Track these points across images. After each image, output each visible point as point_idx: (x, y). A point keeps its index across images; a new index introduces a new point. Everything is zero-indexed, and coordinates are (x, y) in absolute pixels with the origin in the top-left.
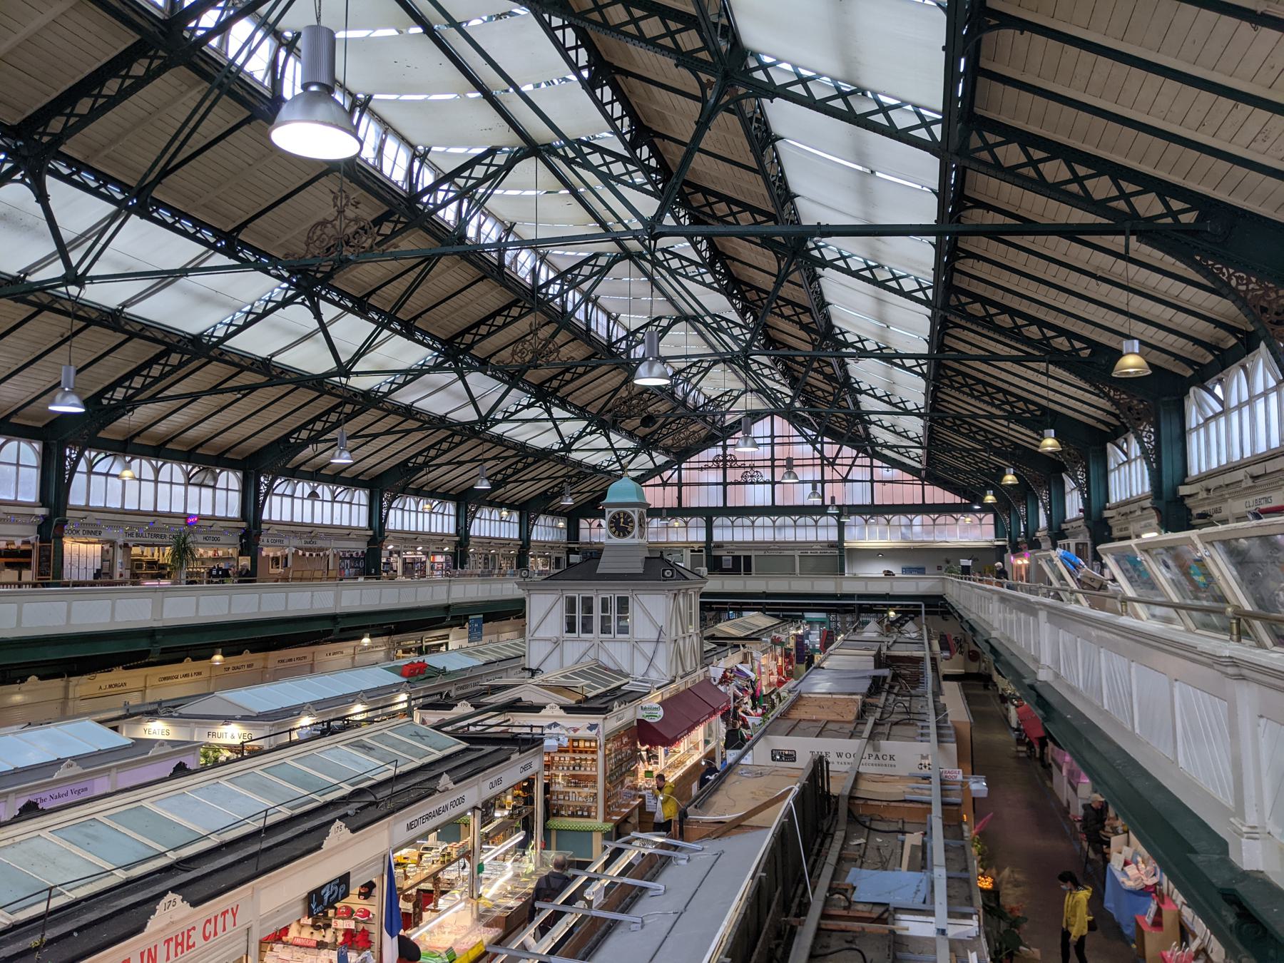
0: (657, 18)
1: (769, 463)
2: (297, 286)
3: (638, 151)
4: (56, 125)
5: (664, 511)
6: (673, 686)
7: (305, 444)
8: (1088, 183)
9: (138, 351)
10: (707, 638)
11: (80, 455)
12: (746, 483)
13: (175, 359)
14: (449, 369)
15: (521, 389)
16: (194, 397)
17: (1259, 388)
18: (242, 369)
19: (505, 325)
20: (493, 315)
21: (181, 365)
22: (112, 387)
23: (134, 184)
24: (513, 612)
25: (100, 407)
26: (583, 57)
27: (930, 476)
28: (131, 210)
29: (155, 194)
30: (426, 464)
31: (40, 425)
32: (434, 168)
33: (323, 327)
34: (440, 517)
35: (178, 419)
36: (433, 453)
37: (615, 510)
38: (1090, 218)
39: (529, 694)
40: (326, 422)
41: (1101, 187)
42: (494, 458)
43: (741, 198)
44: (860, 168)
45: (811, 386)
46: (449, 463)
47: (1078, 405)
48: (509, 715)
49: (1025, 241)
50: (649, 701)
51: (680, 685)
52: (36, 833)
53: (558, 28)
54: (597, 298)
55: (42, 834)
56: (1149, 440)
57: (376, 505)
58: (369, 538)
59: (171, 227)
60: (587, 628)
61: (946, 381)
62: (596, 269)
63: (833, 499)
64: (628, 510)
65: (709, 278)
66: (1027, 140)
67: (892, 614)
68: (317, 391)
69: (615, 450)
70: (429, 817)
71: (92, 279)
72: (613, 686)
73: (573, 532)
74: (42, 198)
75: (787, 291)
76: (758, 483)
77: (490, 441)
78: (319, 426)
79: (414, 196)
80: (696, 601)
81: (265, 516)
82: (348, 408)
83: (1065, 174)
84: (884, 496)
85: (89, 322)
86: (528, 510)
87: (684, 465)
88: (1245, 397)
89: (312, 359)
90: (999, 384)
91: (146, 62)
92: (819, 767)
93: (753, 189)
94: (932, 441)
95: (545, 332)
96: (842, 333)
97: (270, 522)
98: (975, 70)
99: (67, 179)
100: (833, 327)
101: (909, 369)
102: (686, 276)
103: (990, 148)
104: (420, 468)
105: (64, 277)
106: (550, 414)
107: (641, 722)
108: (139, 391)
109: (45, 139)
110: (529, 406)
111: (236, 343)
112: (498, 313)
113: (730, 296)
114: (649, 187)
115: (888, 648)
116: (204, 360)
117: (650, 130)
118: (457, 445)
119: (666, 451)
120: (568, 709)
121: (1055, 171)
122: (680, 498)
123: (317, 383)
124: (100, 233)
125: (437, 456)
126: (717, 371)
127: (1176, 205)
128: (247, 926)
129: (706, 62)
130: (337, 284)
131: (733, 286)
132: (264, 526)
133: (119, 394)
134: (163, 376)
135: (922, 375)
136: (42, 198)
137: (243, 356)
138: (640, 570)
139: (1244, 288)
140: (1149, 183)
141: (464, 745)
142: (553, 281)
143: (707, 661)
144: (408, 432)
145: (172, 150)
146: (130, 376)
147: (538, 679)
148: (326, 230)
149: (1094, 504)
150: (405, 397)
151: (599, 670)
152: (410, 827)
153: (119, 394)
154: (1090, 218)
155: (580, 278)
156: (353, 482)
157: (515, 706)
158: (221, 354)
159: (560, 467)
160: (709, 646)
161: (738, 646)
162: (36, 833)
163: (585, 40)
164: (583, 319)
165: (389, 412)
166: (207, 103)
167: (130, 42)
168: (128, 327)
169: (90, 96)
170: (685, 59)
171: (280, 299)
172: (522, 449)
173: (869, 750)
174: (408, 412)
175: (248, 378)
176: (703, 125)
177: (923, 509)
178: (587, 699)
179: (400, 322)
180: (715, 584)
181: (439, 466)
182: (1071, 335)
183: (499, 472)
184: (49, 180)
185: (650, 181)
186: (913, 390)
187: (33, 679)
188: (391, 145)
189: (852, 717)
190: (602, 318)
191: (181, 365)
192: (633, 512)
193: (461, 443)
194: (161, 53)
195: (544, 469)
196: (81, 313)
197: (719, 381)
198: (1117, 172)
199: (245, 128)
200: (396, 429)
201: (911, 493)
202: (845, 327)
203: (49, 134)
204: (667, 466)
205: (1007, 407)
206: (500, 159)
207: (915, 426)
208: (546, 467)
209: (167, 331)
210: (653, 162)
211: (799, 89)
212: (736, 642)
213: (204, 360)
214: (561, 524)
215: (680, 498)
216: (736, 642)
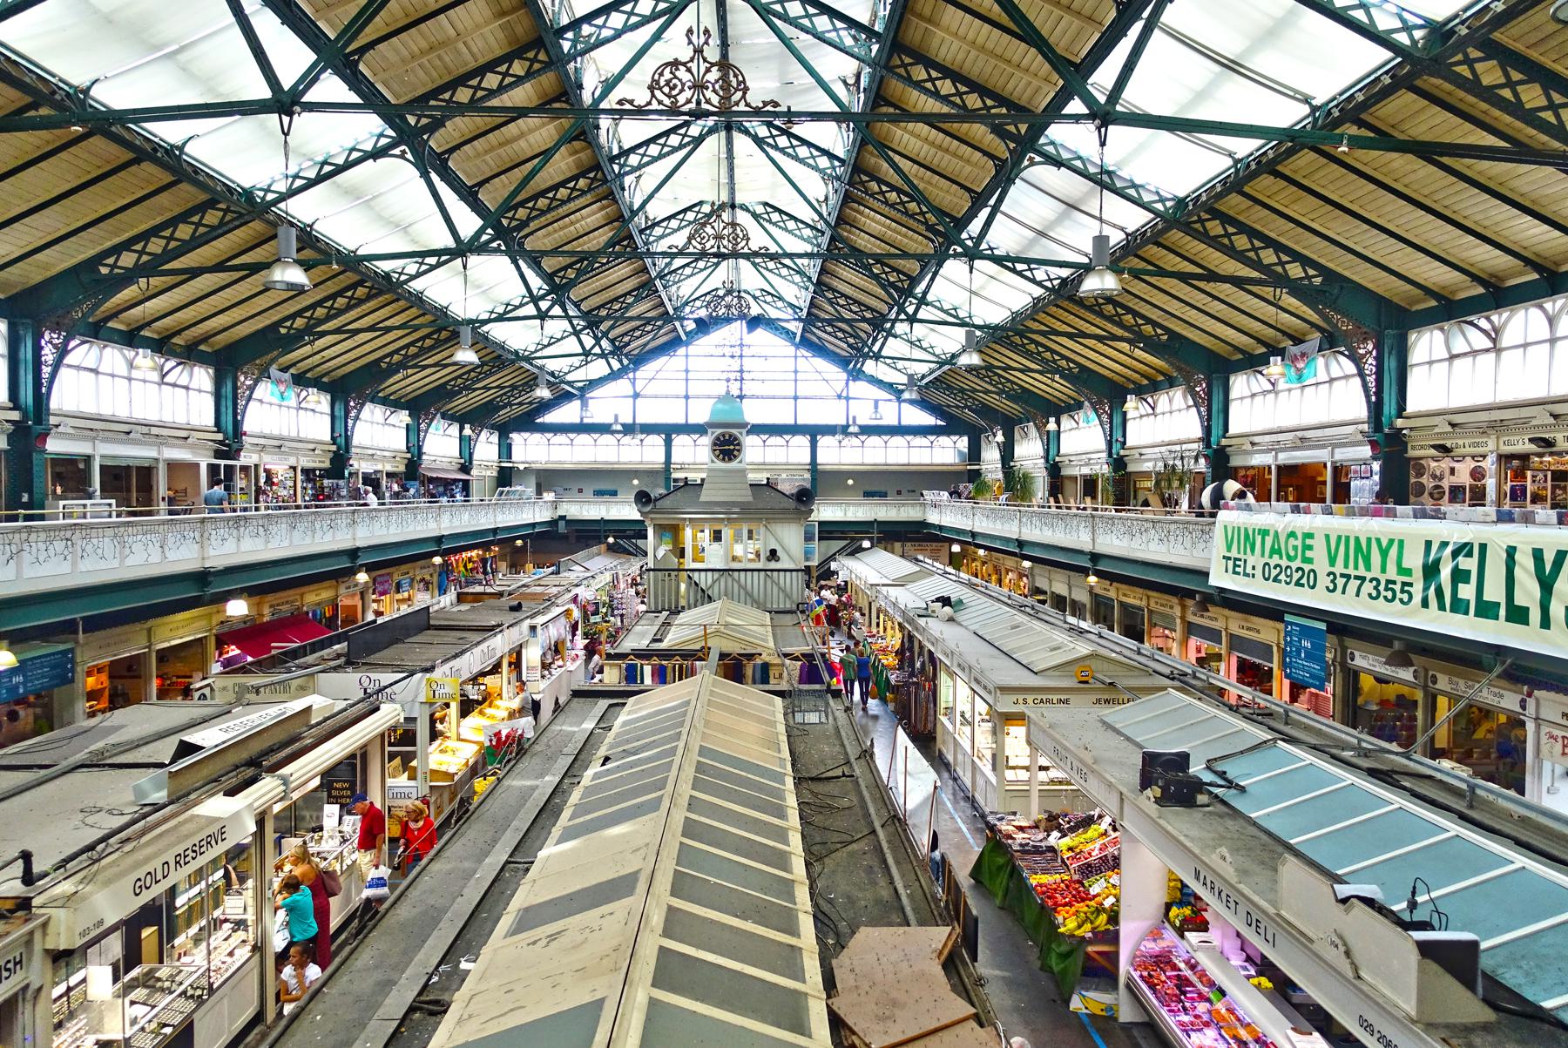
7: (129, 277)
13: (212, 217)
14: (497, 250)
16: (194, 273)
37: (719, 431)
38: (1255, 274)
40: (170, 238)
41: (1268, 256)
49: (1209, 287)
58: (331, 455)
62: (687, 140)
63: (854, 418)
78: (156, 246)
101: (1020, 274)
102: (776, 147)
121: (1242, 242)
125: (328, 318)
127: (1311, 272)
140: (1297, 257)
148: (677, 73)
154: (1255, 274)
182: (1068, 359)
198: (1279, 247)
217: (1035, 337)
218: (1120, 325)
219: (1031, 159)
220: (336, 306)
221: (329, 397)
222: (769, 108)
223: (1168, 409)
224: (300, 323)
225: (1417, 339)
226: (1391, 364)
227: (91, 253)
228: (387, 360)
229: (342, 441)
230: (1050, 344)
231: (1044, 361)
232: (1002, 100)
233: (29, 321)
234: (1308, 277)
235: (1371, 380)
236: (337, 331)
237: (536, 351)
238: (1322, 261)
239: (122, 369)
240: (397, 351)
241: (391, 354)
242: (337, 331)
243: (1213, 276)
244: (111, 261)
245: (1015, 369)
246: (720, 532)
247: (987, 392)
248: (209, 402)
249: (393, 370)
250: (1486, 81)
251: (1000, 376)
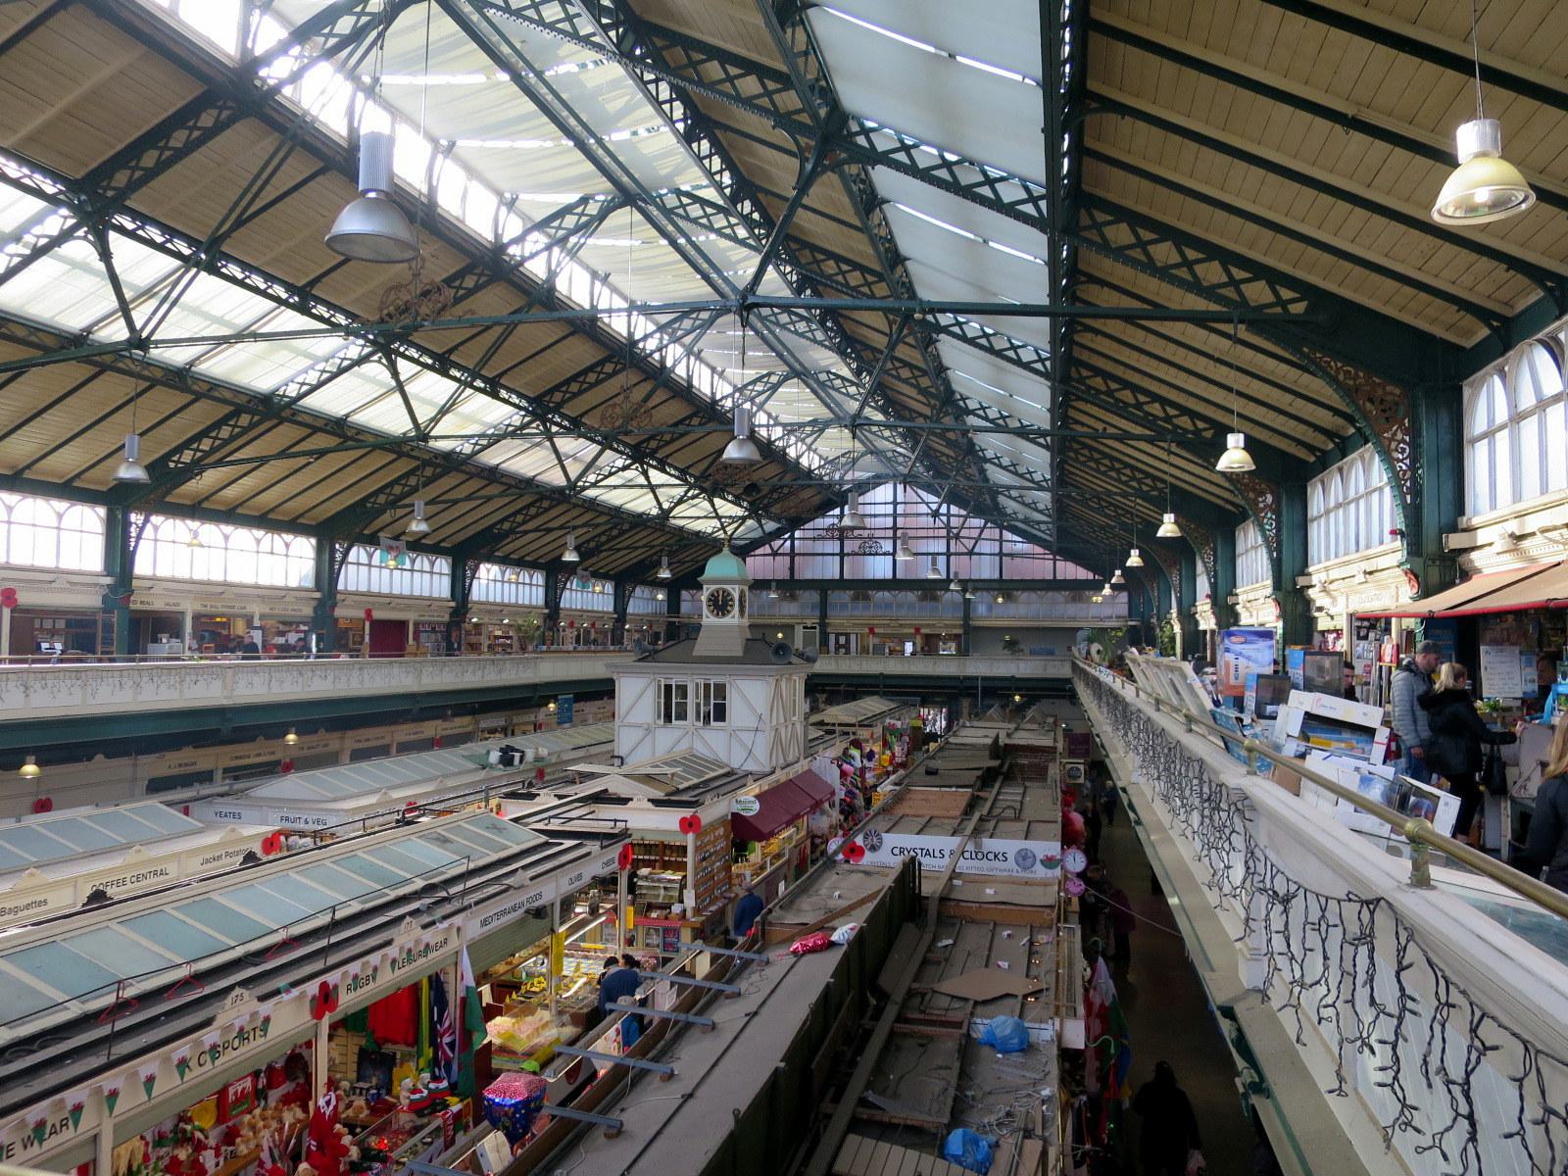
1: (890, 533)
2: (373, 343)
3: (739, 206)
4: (121, 178)
5: (774, 584)
6: (773, 777)
7: (381, 511)
8: (1198, 268)
9: (203, 413)
10: (813, 724)
11: (146, 521)
12: (865, 554)
13: (245, 420)
15: (616, 450)
16: (263, 461)
18: (315, 430)
19: (598, 382)
20: (585, 372)
21: (252, 426)
22: (179, 449)
23: (203, 239)
24: (603, 690)
26: (678, 110)
27: (1063, 548)
28: (198, 264)
29: (224, 248)
30: (512, 531)
31: (104, 489)
32: (523, 216)
33: (400, 387)
34: (527, 588)
35: (248, 483)
36: (519, 518)
37: (713, 587)
39: (616, 784)
42: (584, 525)
43: (850, 256)
44: (971, 236)
45: (935, 450)
46: (536, 530)
47: (1205, 486)
48: (594, 807)
50: (746, 794)
51: (781, 776)
52: (104, 925)
53: (650, 82)
54: (700, 351)
55: (109, 924)
56: (1270, 526)
57: (459, 572)
58: (314, 603)
59: (241, 283)
60: (682, 716)
61: (1072, 454)
63: (956, 574)
65: (820, 336)
66: (1135, 220)
67: (1017, 698)
68: (394, 452)
69: (718, 517)
70: (504, 913)
71: (157, 342)
72: (707, 777)
73: (674, 604)
74: (105, 255)
75: (902, 352)
76: (877, 554)
77: (582, 506)
78: (397, 490)
79: (500, 248)
80: (800, 687)
81: (341, 587)
82: (429, 471)
83: (1175, 258)
84: (1016, 570)
85: (154, 383)
86: (625, 580)
87: (797, 534)
88: (1362, 490)
89: (390, 419)
90: (1126, 459)
91: (214, 112)
92: (910, 871)
93: (859, 247)
94: (1060, 508)
95: (638, 394)
96: (964, 399)
97: (347, 593)
98: (1078, 151)
99: (131, 235)
100: (953, 392)
103: (1098, 227)
104: (506, 534)
105: (128, 341)
106: (647, 478)
107: (735, 815)
108: (207, 454)
109: (110, 193)
110: (625, 468)
111: (313, 402)
112: (591, 369)
113: (842, 354)
114: (751, 241)
115: (1009, 735)
116: (275, 421)
117: (753, 184)
118: (546, 510)
119: (776, 519)
120: (657, 802)
121: (1164, 252)
122: (792, 569)
123: (393, 445)
124: (167, 295)
125: (524, 522)
126: (831, 432)
127: (1286, 294)
128: (94, 1132)
129: (805, 125)
130: (416, 341)
131: (848, 344)
132: (339, 597)
133: (187, 456)
134: (233, 438)
135: (1046, 447)
136: (105, 255)
137: (316, 415)
138: (739, 653)
139: (1351, 382)
140: (1260, 271)
141: (543, 838)
142: (651, 335)
143: (812, 751)
144: (489, 499)
145: (244, 203)
146: (198, 437)
147: (625, 769)
149: (1221, 592)
150: (492, 457)
151: (691, 761)
152: (484, 923)
153: (187, 456)
155: (680, 333)
156: (435, 550)
157: (601, 798)
158: (293, 415)
159: (658, 534)
160: (814, 733)
161: (848, 733)
162: (104, 925)
163: (679, 93)
164: (684, 375)
165: (471, 476)
166: (281, 154)
167: (197, 93)
168: (195, 388)
169: (157, 148)
170: (783, 120)
172: (616, 513)
173: (970, 847)
174: (493, 474)
175: (321, 441)
176: (804, 184)
177: (1055, 585)
178: (678, 792)
179: (485, 379)
180: (825, 666)
181: (526, 532)
182: (1194, 415)
183: (592, 539)
184: (113, 236)
185: (752, 234)
186: (1038, 459)
187: (99, 757)
188: (477, 189)
189: (958, 813)
190: (706, 372)
191: (252, 426)
193: (551, 507)
194: (230, 104)
195: (640, 537)
196: (146, 373)
197: (837, 442)
199: (319, 179)
200: (293, 450)
201: (1043, 567)
202: (966, 393)
203: (114, 189)
204: (777, 534)
205: (1134, 484)
206: (593, 209)
207: (1044, 498)
208: (644, 533)
209: (237, 391)
210: (756, 216)
211: (901, 157)
212: (846, 729)
213: (275, 421)
214: (660, 597)
215: (792, 569)
216: (846, 729)
217: (1199, 304)
218: (1196, 287)
221: (313, 541)
222: (468, 316)
224: (506, 526)
227: (162, 452)
231: (1148, 421)
239: (427, 567)
246: (721, 690)
247: (1124, 437)
248: (541, 591)
251: (1091, 449)
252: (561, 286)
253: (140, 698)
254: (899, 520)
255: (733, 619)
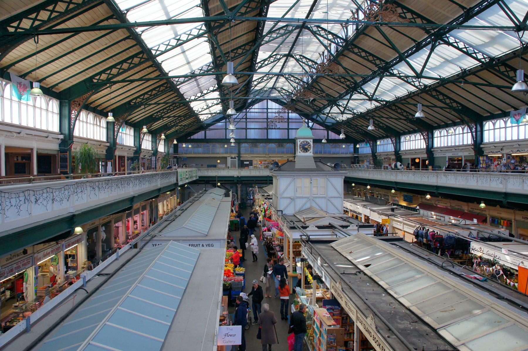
0: (241, 326)
16: (76, 31)
17: (417, 139)
25: (92, 84)
34: (85, 124)
36: (114, 71)
37: (302, 140)
41: (448, 101)
56: (371, 145)
64: (308, 140)
121: (441, 97)
125: (119, 74)
127: (459, 105)
140: (455, 101)
171: (196, 34)
182: (383, 123)
192: (311, 141)
198: (450, 99)
217: (405, 118)
218: (402, 115)
219: (439, 42)
220: (133, 62)
223: (414, 139)
225: (486, 123)
226: (479, 128)
228: (134, 101)
229: (66, 131)
230: (381, 121)
232: (429, 22)
233: (66, 101)
234: (458, 107)
235: (474, 134)
236: (123, 81)
237: (202, 111)
238: (462, 103)
239: (44, 106)
240: (146, 93)
241: (136, 98)
242: (123, 81)
243: (436, 106)
244: (15, 24)
245: (377, 117)
249: (137, 106)
250: (502, 70)
252: (465, 67)
253: (467, 184)
254: (269, 114)
255: (310, 154)
